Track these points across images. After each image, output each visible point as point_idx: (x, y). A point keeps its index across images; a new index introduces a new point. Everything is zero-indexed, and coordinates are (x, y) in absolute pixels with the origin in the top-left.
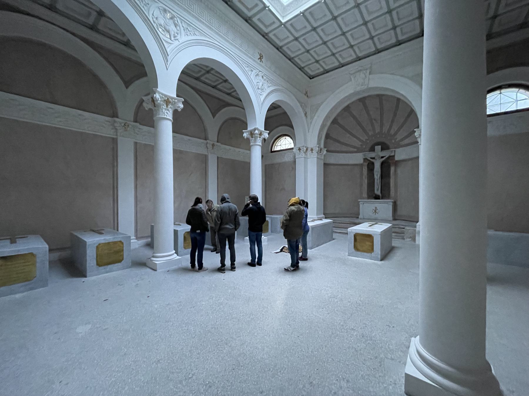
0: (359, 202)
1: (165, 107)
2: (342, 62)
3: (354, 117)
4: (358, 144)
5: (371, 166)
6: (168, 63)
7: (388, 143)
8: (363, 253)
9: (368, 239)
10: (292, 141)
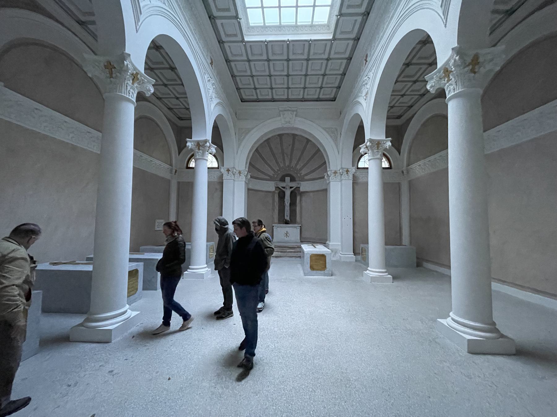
1: (131, 84)
3: (271, 148)
4: (271, 173)
5: (282, 196)
6: (139, 24)
7: (295, 175)
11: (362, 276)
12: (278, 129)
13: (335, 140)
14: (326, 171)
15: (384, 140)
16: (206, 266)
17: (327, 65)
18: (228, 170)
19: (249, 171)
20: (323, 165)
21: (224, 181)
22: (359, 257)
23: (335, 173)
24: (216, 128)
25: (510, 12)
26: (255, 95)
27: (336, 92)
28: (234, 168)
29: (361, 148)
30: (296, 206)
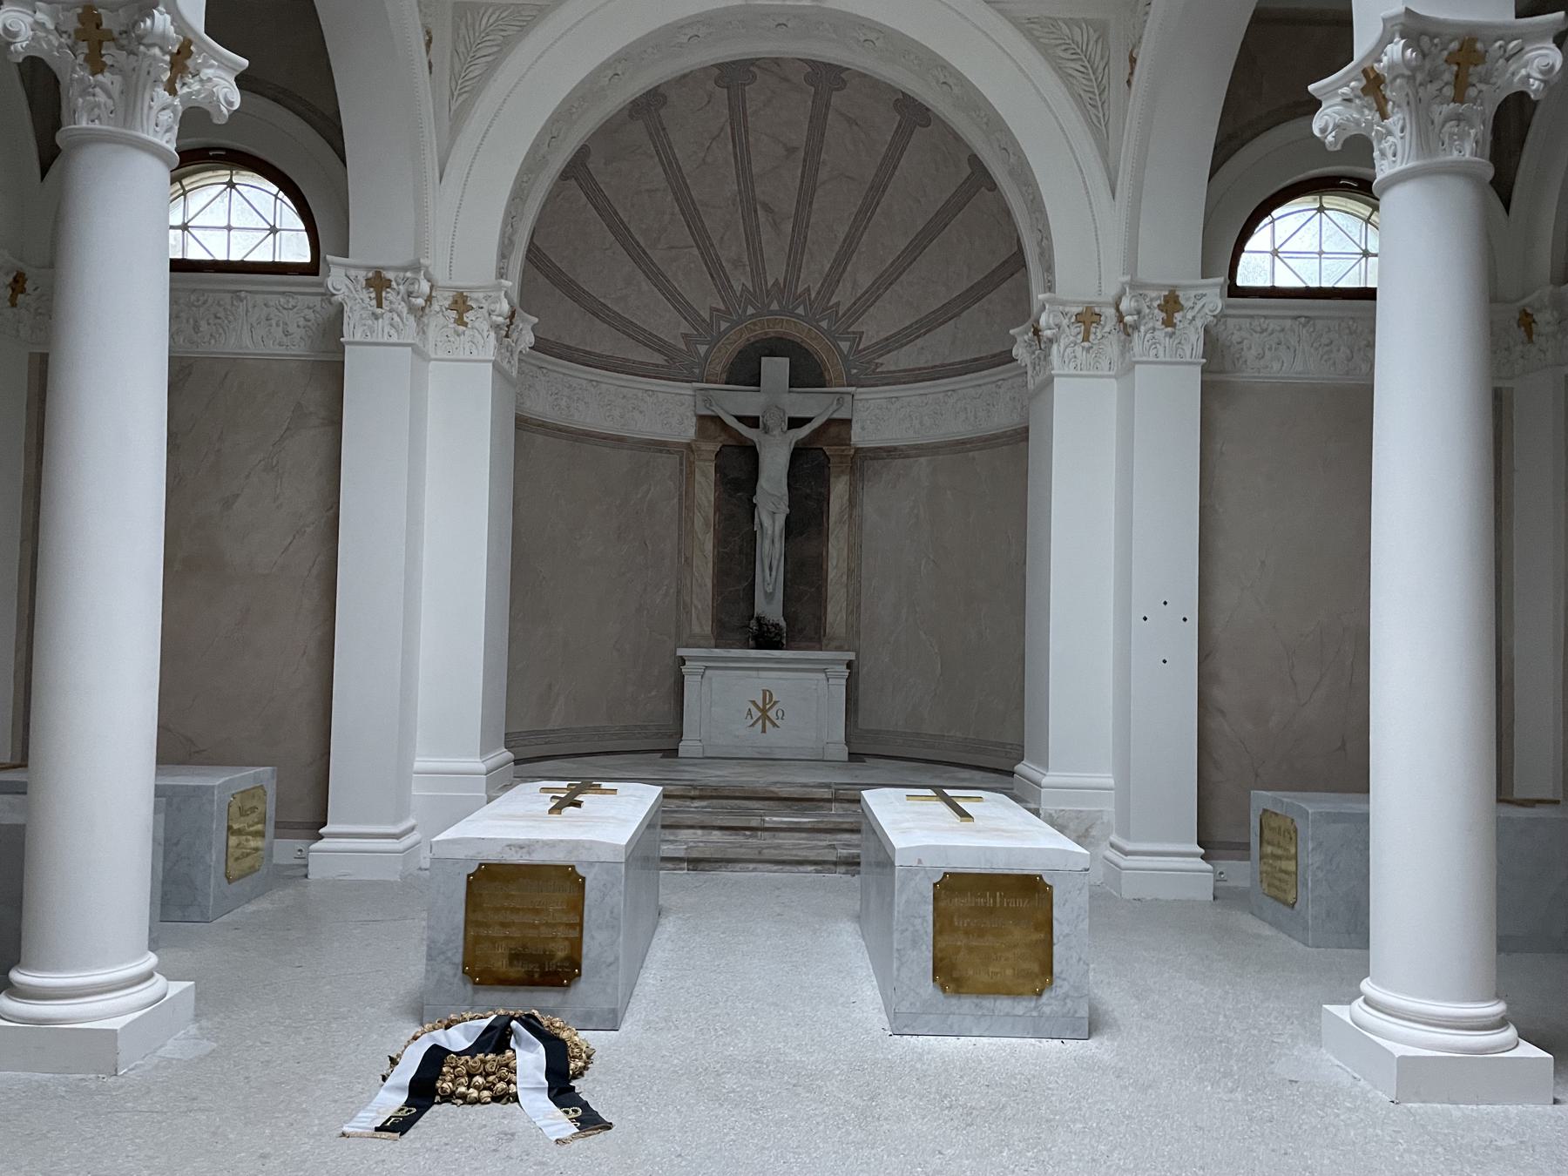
0: (683, 661)
3: (670, 166)
5: (738, 466)
8: (988, 1003)
9: (1022, 904)
10: (290, 217)
11: (1316, 1038)
13: (1096, 109)
16: (151, 960)
19: (527, 300)
20: (1008, 272)
21: (351, 358)
22: (1240, 873)
23: (1088, 319)
28: (416, 267)
29: (1314, 105)
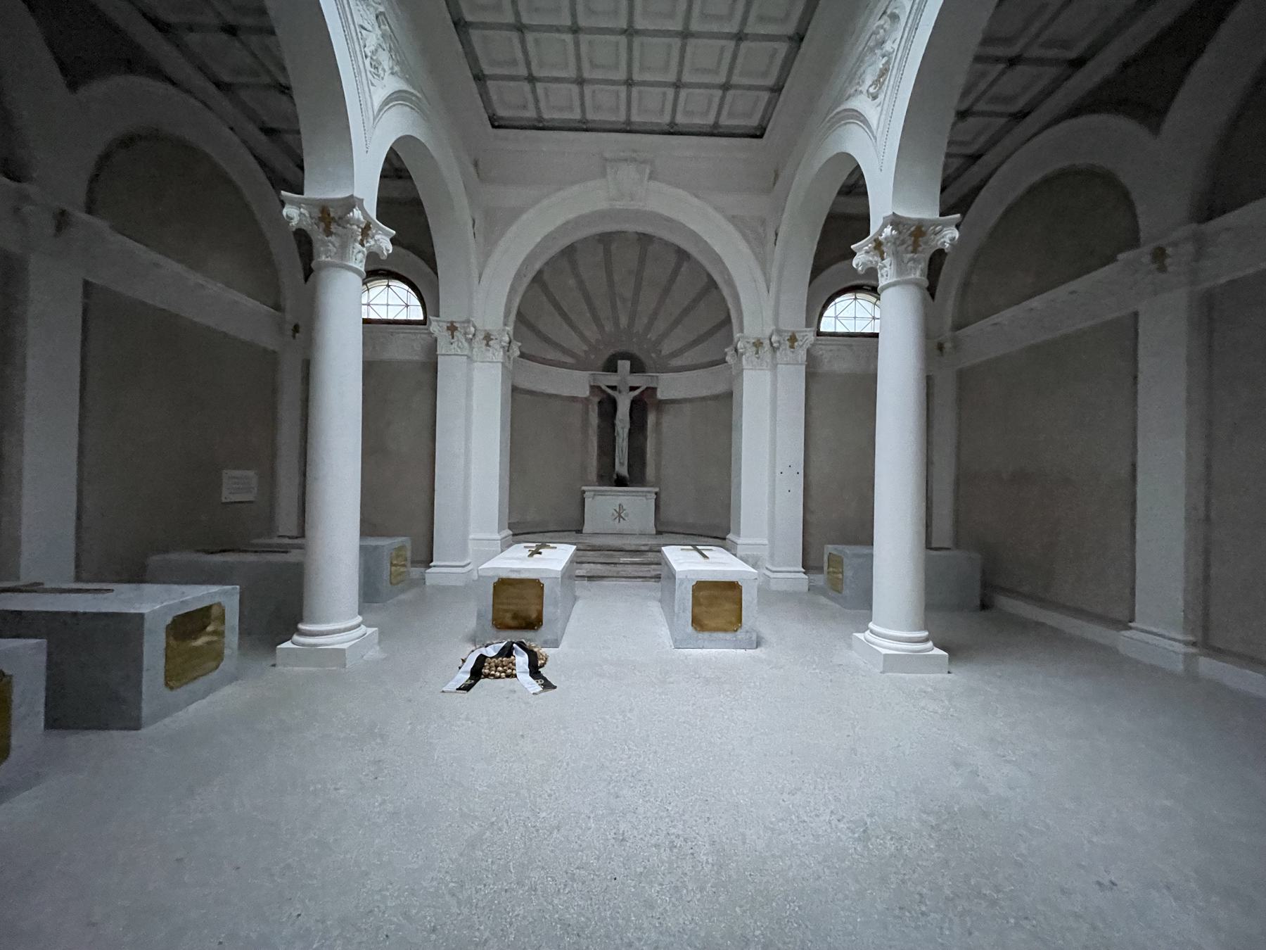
0: (584, 492)
2: (590, 116)
5: (608, 407)
10: (414, 300)
11: (850, 647)
12: (602, 215)
14: (729, 340)
15: (934, 223)
16: (359, 619)
17: (734, 57)
18: (452, 328)
20: (724, 325)
21: (440, 359)
22: (820, 579)
23: (758, 344)
24: (394, 170)
25: (1021, 116)
26: (531, 106)
27: (769, 102)
28: (468, 321)
29: (854, 254)
30: (645, 438)
